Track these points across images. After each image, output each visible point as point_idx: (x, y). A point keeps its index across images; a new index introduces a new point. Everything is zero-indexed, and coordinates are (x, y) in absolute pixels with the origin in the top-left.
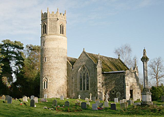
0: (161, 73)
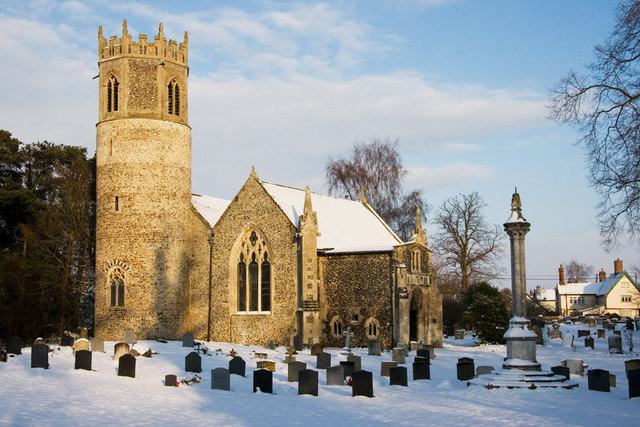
0: (476, 246)
